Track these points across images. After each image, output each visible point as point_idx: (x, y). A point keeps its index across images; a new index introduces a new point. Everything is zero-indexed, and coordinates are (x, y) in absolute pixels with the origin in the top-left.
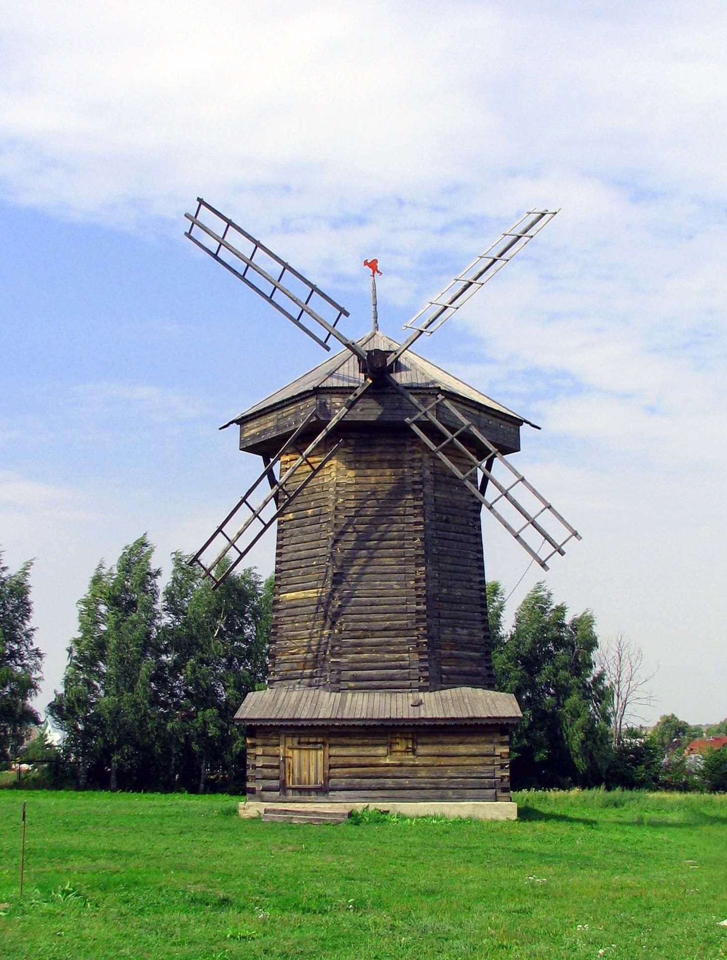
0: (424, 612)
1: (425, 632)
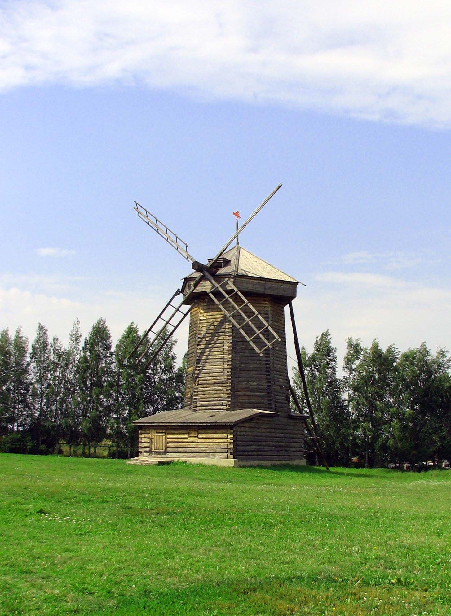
0: (230, 376)
1: (230, 384)
